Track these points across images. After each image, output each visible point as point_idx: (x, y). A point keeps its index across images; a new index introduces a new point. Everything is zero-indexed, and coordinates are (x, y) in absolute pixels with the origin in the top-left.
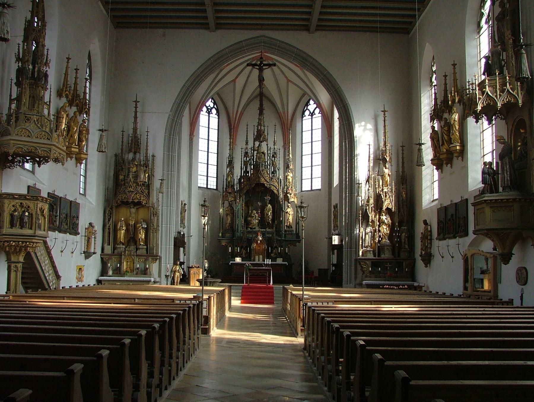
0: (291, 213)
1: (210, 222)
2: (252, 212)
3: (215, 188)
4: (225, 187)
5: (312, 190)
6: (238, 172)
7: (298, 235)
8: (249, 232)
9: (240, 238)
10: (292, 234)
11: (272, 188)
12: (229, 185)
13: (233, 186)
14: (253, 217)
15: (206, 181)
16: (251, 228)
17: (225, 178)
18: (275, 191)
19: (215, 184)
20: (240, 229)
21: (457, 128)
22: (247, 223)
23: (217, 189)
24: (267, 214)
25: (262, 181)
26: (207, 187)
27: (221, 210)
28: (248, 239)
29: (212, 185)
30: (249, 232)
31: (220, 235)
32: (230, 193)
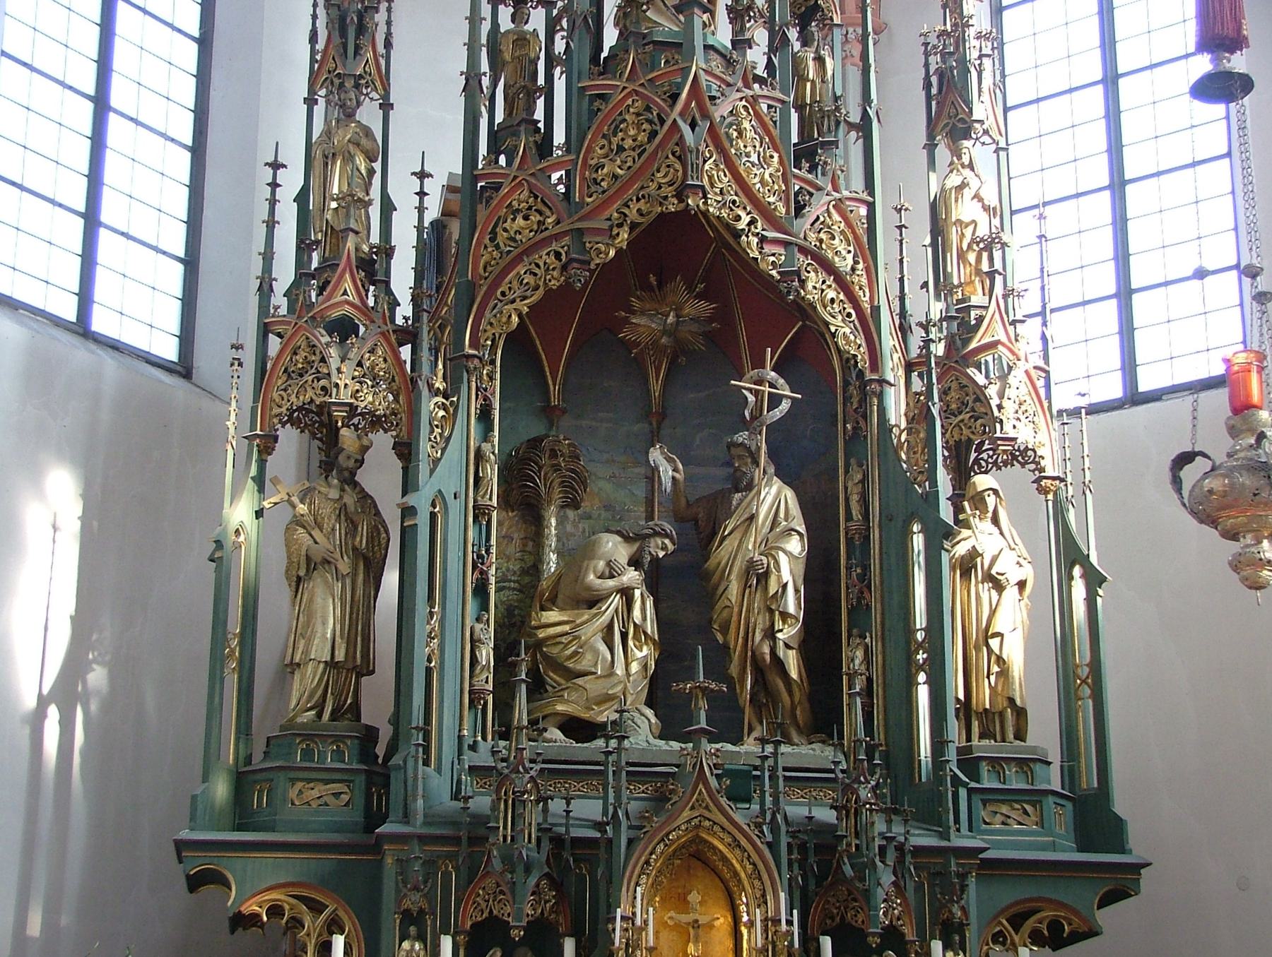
0: (1011, 567)
1: (97, 677)
2: (576, 556)
3: (169, 350)
4: (285, 274)
5: (1134, 398)
6: (427, 138)
7: (1095, 818)
8: (560, 772)
9: (467, 838)
10: (1036, 797)
11: (815, 285)
12: (335, 247)
13: (373, 268)
14: (593, 601)
15: (74, 266)
16: (578, 729)
17: (292, 180)
18: (844, 330)
19: (172, 320)
20: (450, 719)
21: (794, 674)
22: (525, 663)
23: (184, 369)
24: (758, 576)
25: (716, 197)
26: (82, 328)
27: (240, 512)
28: (557, 843)
29: (141, 308)
30: (560, 772)
31: (221, 789)
32: (344, 329)
